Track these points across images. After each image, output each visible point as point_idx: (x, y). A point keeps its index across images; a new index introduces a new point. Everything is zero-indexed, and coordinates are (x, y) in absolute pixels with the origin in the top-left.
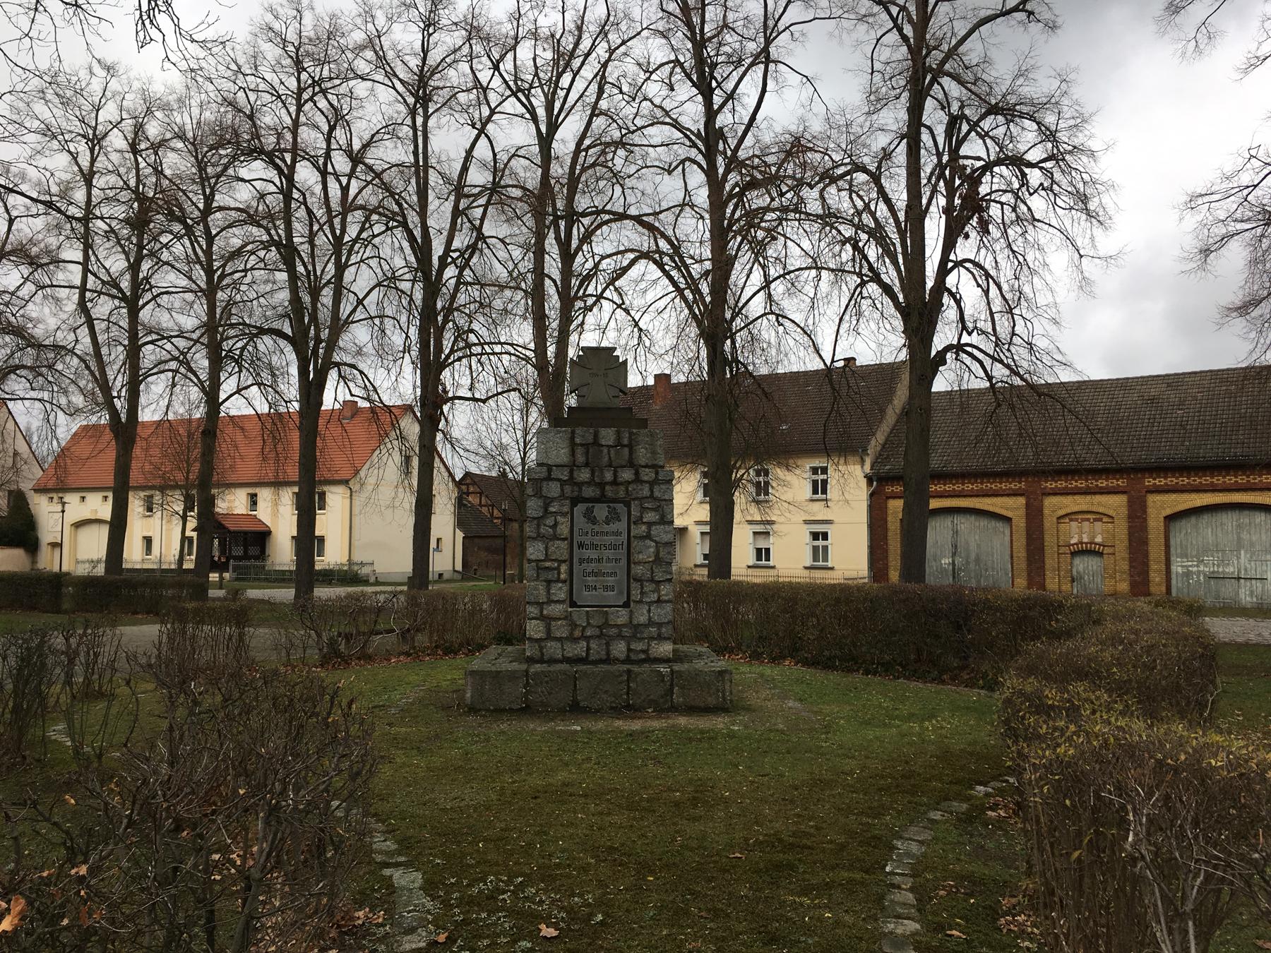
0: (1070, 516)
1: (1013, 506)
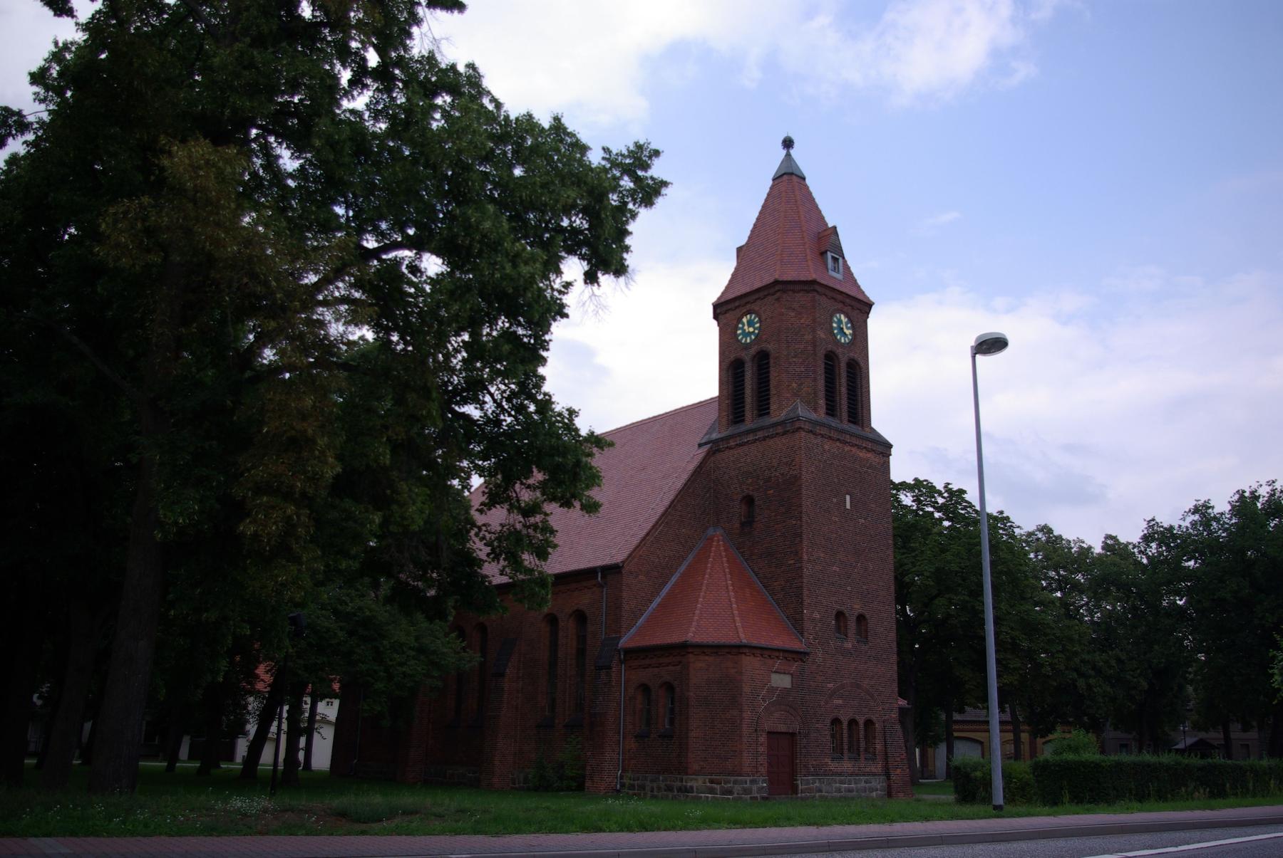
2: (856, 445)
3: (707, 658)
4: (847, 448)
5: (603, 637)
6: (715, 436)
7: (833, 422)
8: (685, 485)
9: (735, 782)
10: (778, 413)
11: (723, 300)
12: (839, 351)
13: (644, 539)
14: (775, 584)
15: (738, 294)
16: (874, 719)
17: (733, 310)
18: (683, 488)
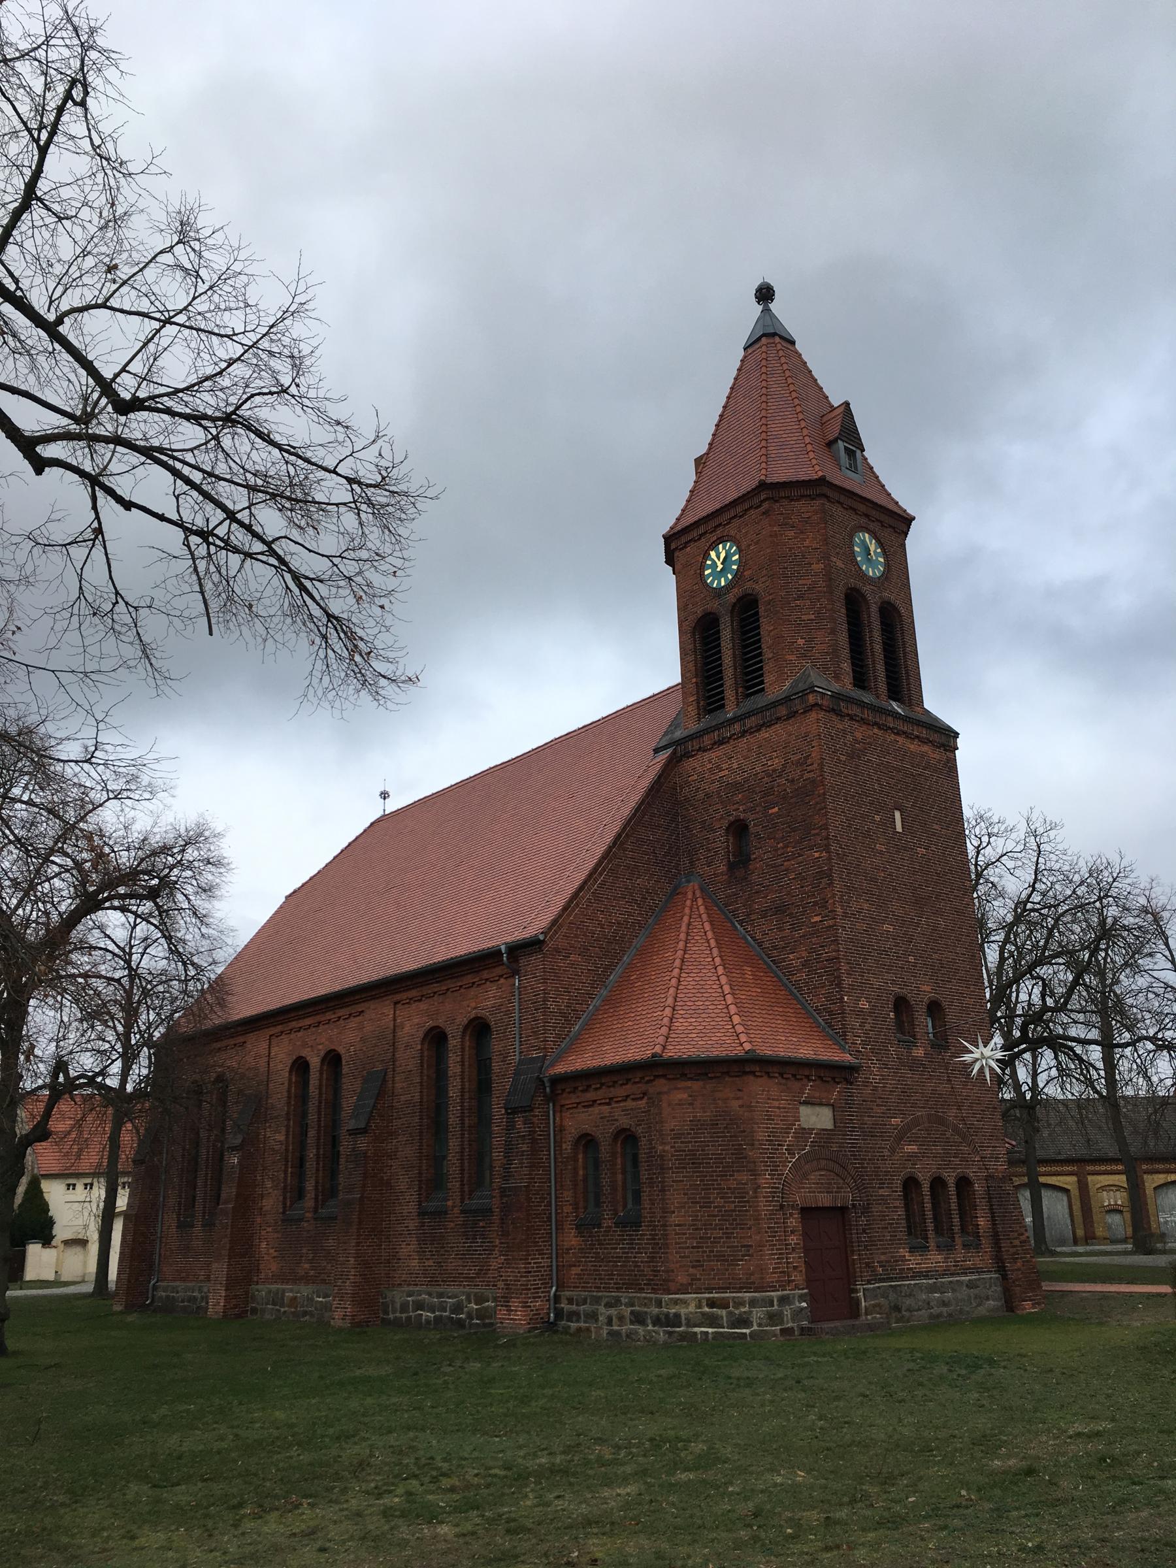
0: (1103, 1188)
1: (1069, 1182)
2: (904, 733)
3: (689, 1083)
4: (900, 739)
5: (517, 1057)
6: (678, 734)
7: (867, 698)
8: (637, 810)
9: (753, 1303)
10: (776, 687)
11: (679, 528)
12: (867, 589)
13: (575, 895)
14: (791, 956)
15: (704, 514)
17: (695, 541)
18: (634, 815)
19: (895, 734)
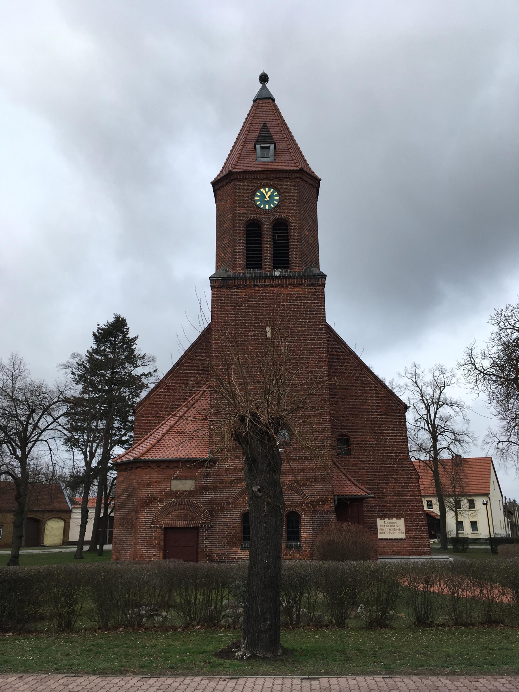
3: (123, 473)
4: (276, 289)
16: (298, 510)
19: (271, 287)
